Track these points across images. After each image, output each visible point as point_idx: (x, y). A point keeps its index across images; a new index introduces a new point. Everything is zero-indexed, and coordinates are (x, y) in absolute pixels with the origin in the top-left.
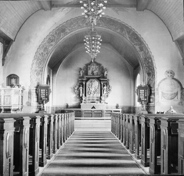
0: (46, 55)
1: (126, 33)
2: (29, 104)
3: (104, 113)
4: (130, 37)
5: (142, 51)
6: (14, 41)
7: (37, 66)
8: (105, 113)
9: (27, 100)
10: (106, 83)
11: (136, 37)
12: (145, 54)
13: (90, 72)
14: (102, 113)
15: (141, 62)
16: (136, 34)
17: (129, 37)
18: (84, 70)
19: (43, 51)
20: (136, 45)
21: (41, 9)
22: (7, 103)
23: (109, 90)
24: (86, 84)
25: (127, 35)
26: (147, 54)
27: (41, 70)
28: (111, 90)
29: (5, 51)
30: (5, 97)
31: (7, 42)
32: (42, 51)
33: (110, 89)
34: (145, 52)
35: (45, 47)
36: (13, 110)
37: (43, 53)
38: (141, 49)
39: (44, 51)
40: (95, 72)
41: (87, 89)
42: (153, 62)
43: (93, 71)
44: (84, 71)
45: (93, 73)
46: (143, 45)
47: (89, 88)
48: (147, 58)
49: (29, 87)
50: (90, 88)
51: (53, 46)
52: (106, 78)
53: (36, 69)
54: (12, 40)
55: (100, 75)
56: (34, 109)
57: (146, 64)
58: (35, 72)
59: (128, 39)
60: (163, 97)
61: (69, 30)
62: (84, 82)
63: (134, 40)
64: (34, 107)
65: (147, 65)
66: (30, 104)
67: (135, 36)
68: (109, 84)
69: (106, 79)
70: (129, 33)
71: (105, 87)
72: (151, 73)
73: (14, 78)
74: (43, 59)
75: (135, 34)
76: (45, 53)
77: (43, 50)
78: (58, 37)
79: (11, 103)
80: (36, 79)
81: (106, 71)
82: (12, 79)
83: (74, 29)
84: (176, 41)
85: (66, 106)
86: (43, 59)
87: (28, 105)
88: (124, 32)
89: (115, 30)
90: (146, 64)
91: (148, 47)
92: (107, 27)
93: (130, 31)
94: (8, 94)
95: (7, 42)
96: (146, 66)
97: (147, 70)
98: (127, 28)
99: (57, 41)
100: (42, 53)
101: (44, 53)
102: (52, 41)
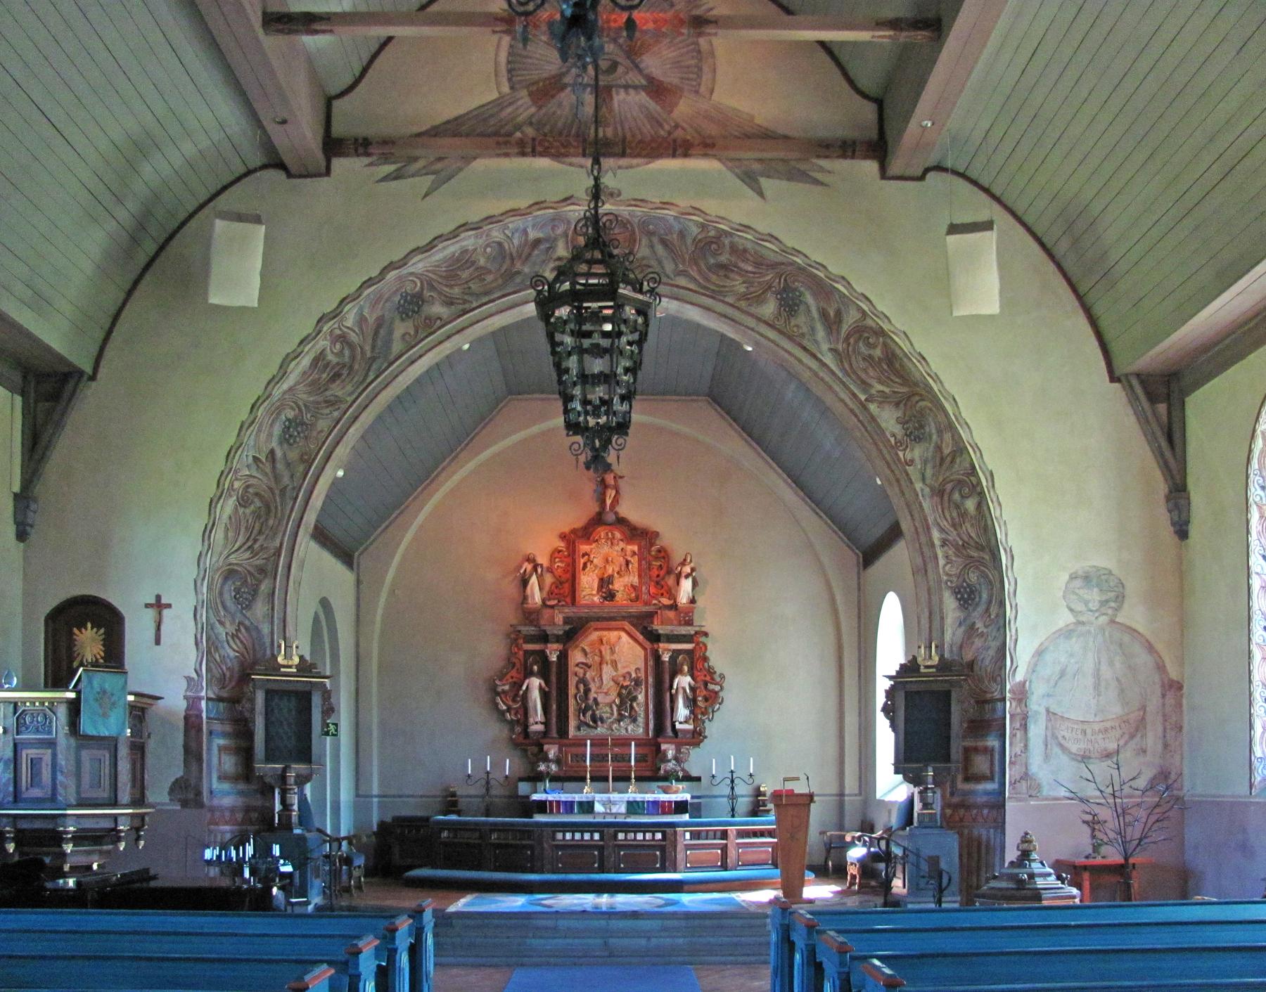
0: (301, 468)
1: (819, 327)
2: (191, 796)
3: (680, 847)
4: (840, 347)
5: (918, 439)
6: (93, 378)
7: (241, 540)
8: (688, 847)
9: (179, 772)
10: (689, 653)
11: (878, 353)
12: (942, 460)
13: (588, 583)
14: (669, 849)
15: (833, 373)
16: (881, 332)
17: (831, 350)
18: (550, 570)
19: (281, 443)
20: (884, 399)
21: (264, 167)
22: (36, 793)
23: (706, 699)
24: (563, 656)
25: (821, 333)
26: (953, 461)
27: (270, 567)
28: (721, 694)
29: (36, 445)
30: (27, 754)
31: (50, 389)
32: (274, 444)
33: (717, 688)
34: (939, 448)
35: (291, 414)
36: (78, 839)
37: (279, 454)
38: (915, 431)
39: (287, 439)
40: (618, 585)
41: (572, 691)
42: (995, 512)
43: (611, 577)
44: (549, 579)
45: (605, 583)
46: (922, 404)
47: (582, 687)
48: (949, 487)
49: (189, 679)
50: (593, 687)
51: (344, 406)
52: (689, 623)
53: (233, 559)
54: (81, 373)
55: (646, 604)
56: (227, 828)
57: (944, 524)
58: (226, 579)
59: (829, 359)
60: (1057, 750)
61: (449, 302)
62: (555, 646)
63: (865, 370)
64: (227, 814)
65: (953, 535)
66: (199, 793)
67: (874, 346)
68: (705, 659)
69: (691, 630)
70: (832, 323)
71: (684, 681)
72: (978, 577)
73: (97, 625)
74: (277, 492)
75: (876, 333)
76: (293, 455)
77: (277, 430)
78: (373, 347)
79: (60, 790)
80: (231, 629)
81: (690, 580)
82: (80, 630)
83: (478, 295)
84: (1135, 382)
85: (510, 797)
86: (277, 492)
87: (185, 804)
88: (801, 320)
89: (743, 304)
90: (942, 530)
91: (958, 415)
92: (692, 286)
93: (838, 313)
94: (37, 731)
95: (50, 389)
96: (944, 543)
97: (954, 571)
98: (823, 289)
99: (367, 375)
100: (272, 452)
101: (285, 455)
102: (337, 376)
